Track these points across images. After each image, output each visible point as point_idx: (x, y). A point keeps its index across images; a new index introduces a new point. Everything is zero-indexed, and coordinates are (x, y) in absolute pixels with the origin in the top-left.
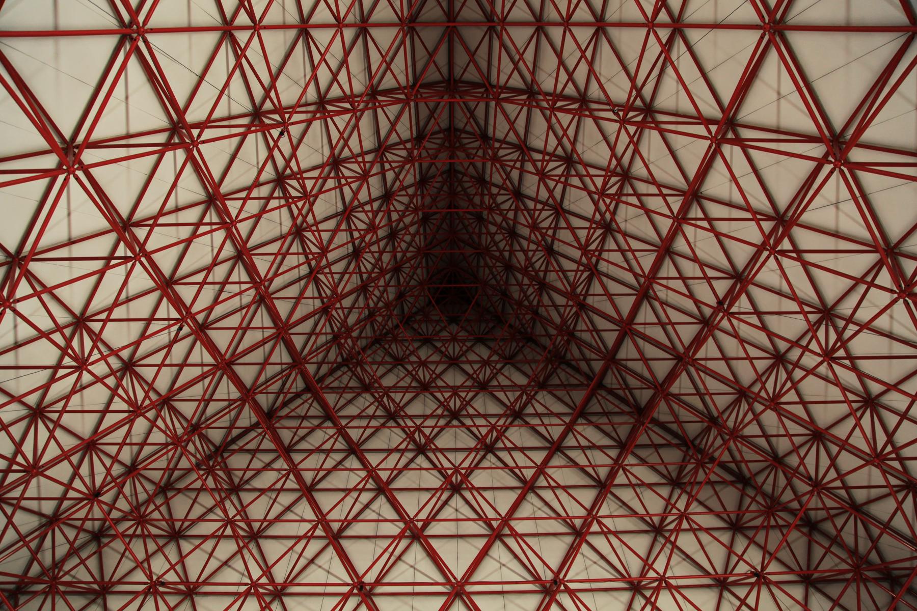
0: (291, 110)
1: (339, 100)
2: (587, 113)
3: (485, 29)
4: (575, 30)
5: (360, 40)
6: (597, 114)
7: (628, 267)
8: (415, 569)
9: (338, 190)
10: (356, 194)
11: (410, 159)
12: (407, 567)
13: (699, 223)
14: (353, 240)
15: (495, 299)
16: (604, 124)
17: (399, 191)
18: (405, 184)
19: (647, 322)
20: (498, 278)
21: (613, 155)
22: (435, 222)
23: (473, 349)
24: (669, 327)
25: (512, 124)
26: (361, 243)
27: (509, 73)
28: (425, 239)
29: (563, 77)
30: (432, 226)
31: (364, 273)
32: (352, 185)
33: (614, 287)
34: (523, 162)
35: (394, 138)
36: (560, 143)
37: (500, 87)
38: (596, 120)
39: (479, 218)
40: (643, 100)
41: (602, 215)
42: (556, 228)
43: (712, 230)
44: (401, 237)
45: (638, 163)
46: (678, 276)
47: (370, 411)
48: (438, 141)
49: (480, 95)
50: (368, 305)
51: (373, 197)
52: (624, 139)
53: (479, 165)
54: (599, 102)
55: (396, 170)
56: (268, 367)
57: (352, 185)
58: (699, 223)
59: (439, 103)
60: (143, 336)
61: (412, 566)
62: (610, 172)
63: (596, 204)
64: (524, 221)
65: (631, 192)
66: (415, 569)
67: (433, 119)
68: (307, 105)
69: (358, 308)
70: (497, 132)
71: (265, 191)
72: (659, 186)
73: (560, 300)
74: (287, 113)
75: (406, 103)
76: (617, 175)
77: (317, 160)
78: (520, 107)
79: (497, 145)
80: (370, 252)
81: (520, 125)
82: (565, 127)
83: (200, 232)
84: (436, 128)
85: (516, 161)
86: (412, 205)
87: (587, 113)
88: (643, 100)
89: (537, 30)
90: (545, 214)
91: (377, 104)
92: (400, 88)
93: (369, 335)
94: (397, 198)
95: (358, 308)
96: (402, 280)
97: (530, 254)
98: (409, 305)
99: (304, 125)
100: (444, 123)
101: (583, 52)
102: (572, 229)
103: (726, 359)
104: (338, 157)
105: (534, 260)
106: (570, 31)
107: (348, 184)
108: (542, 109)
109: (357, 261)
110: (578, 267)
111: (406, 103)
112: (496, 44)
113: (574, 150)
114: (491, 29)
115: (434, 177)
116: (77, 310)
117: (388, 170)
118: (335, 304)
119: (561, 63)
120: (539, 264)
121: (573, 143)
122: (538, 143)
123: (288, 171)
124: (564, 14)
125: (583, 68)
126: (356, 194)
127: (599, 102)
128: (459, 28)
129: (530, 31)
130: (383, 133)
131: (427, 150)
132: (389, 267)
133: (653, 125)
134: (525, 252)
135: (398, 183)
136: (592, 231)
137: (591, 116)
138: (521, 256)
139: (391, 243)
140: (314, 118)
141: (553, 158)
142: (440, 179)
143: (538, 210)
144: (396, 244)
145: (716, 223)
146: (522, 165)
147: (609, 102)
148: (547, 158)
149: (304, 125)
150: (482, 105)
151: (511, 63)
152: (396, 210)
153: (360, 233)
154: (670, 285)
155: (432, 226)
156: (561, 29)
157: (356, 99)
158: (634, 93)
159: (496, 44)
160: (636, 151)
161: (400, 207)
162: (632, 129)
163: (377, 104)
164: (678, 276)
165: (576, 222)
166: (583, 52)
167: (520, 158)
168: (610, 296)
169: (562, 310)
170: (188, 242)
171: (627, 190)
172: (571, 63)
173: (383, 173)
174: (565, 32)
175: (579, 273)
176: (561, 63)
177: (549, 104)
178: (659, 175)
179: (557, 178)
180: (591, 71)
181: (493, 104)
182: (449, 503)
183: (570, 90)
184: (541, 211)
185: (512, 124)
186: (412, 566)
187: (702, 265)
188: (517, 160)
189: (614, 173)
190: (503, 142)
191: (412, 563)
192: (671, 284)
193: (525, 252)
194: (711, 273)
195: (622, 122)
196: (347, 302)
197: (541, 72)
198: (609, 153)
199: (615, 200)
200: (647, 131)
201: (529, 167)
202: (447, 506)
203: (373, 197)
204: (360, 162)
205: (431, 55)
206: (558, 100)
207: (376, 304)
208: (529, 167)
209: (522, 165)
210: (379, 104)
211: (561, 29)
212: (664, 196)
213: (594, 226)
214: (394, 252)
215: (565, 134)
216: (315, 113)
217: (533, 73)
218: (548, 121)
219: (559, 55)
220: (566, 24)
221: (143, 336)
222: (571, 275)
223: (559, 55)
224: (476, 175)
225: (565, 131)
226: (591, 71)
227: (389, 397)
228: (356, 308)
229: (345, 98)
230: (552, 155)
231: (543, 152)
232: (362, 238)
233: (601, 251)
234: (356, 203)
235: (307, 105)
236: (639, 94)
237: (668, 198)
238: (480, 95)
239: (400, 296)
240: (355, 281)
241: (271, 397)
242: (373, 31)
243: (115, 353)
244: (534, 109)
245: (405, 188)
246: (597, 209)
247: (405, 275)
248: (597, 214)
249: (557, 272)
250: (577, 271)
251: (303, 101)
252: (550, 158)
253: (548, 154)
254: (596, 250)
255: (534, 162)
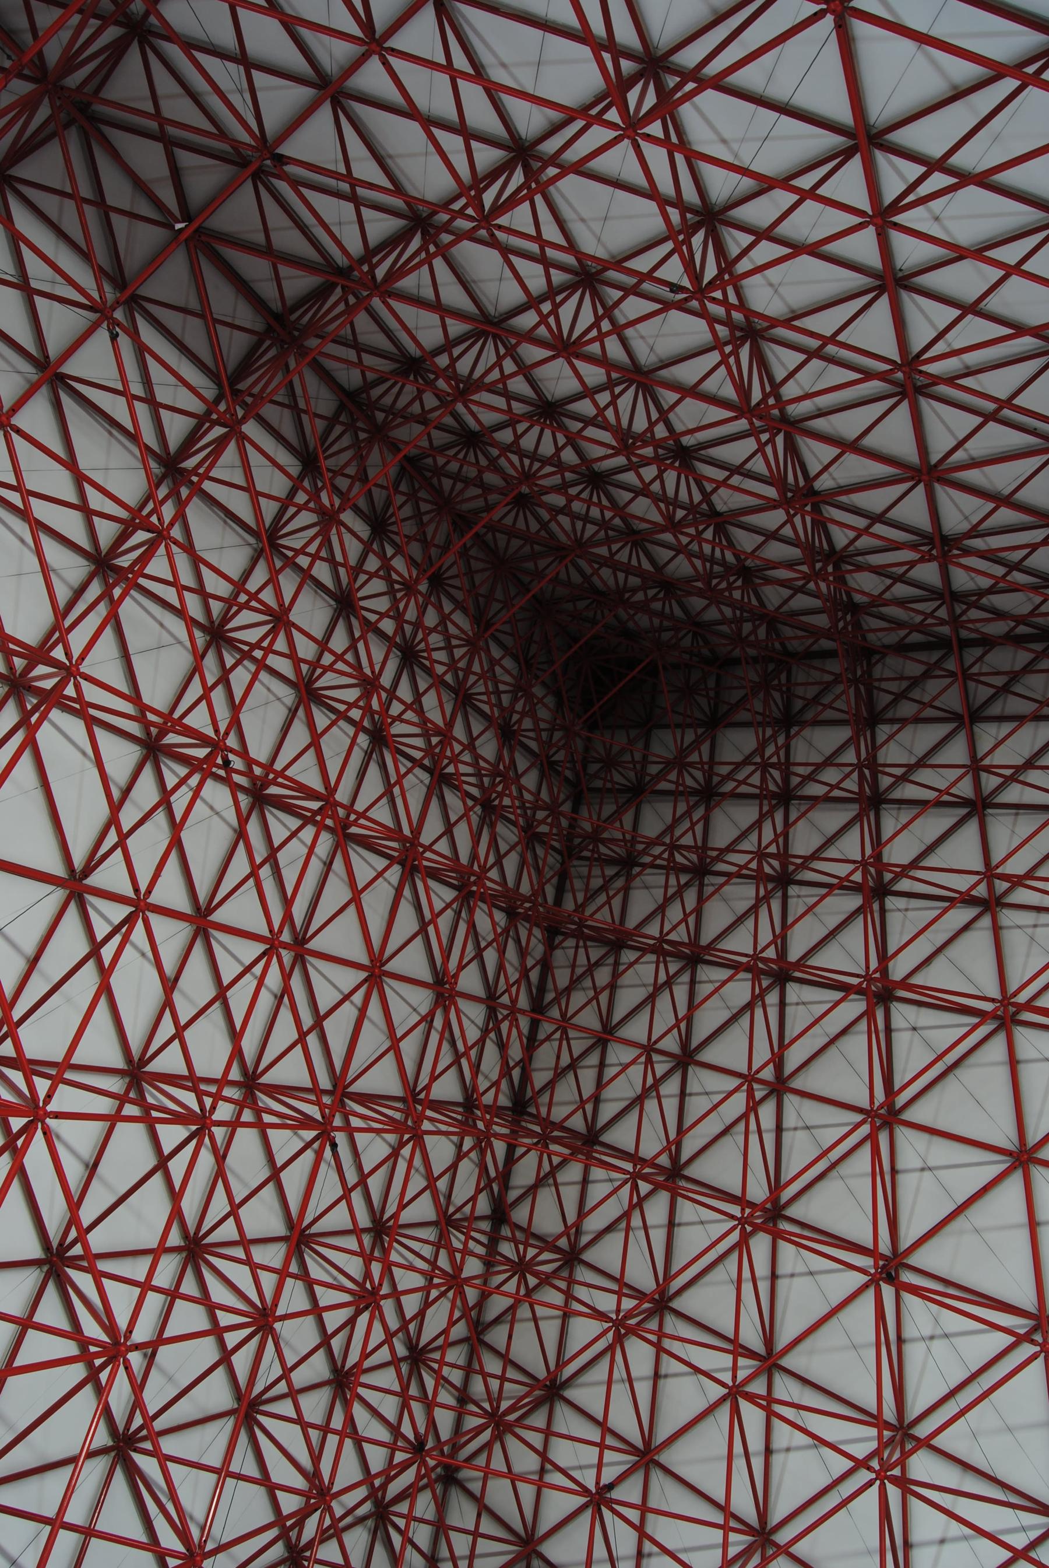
0: (57, 635)
1: (123, 537)
2: (552, 171)
3: (248, 186)
4: (397, 42)
5: (66, 400)
6: (572, 155)
7: (859, 376)
8: (930, 1169)
9: (263, 676)
10: (292, 655)
11: (328, 519)
12: (917, 1174)
13: (923, 190)
14: (357, 725)
15: (623, 556)
16: (602, 164)
17: (355, 580)
18: (353, 561)
19: (961, 437)
20: (595, 512)
21: (663, 202)
22: (454, 571)
23: (717, 759)
24: (1006, 412)
25: (437, 306)
26: (373, 719)
27: (729, 1121)
28: (465, 611)
29: (452, 143)
30: (456, 582)
31: (423, 758)
32: (276, 647)
33: (849, 424)
34: (512, 352)
35: (269, 509)
36: (547, 264)
37: (362, 261)
38: (579, 168)
39: (522, 502)
40: (630, 55)
41: (728, 322)
42: (664, 416)
43: (964, 179)
44: (422, 646)
45: (714, 176)
46: (958, 312)
47: (596, 883)
48: (346, 441)
49: (341, 307)
50: (468, 795)
51: (320, 638)
52: (657, 157)
53: (448, 420)
54: (555, 129)
55: (323, 554)
56: (423, 1183)
57: (276, 647)
58: (923, 190)
59: (291, 383)
60: (176, 1196)
61: (923, 1170)
62: (680, 232)
63: (703, 314)
64: (601, 451)
65: (746, 239)
66: (930, 1169)
67: (303, 416)
68: (79, 592)
69: (489, 944)
70: (421, 337)
71: (146, 792)
72: (785, 183)
73: (772, 519)
74: (35, 709)
75: (234, 432)
76: (694, 229)
77: (180, 660)
78: (426, 268)
79: (443, 361)
80: (395, 719)
81: (453, 295)
82: (533, 232)
83: (107, 959)
84: (320, 424)
85: (499, 364)
86: (397, 586)
87: (552, 171)
88: (630, 55)
89: (336, 105)
90: (625, 402)
91: (195, 479)
92: (202, 421)
93: (514, 839)
94: (360, 594)
95: (489, 944)
96: (486, 708)
97: (656, 487)
98: (532, 734)
99: (109, 632)
100: (324, 402)
101: (448, 68)
102: (693, 392)
103: (972, 309)
104: (212, 622)
105: (670, 491)
106: (393, 51)
107: (269, 650)
108: (470, 236)
109: (387, 747)
110: (758, 441)
111: (234, 432)
112: (299, 911)
113: (580, 256)
114: (259, 177)
115: (388, 503)
116: (33, 1250)
117: (311, 565)
118: (418, 852)
119: (428, 123)
120: (687, 493)
121: (571, 247)
122: (510, 295)
123: (154, 731)
124: (356, 31)
125: (473, 94)
126: (292, 655)
127: (555, 129)
128: (206, 224)
129: (325, 115)
130: (248, 517)
131: (340, 472)
132: (448, 709)
133: (690, 86)
134: (644, 491)
135: (342, 571)
136: (732, 360)
137: (566, 170)
138: (642, 507)
139: (416, 669)
140: (115, 605)
141: (559, 299)
142: (399, 499)
143: (607, 407)
144: (427, 663)
145: (958, 160)
146: (517, 360)
147: (570, 114)
148: (546, 307)
149: (109, 632)
150: (362, 320)
151: (343, 202)
152: (382, 616)
153: (359, 707)
154: (957, 345)
155: (456, 582)
156: (374, 63)
157: (145, 513)
158: (607, 56)
159: (299, 911)
160: (693, 157)
161: (382, 604)
162: (655, 129)
163: (195, 479)
164: (957, 313)
165: (688, 373)
166: (448, 68)
167: (502, 351)
168: (853, 447)
169: (787, 531)
170: (105, 989)
171: (738, 244)
172: (443, 106)
173: (306, 576)
174: (386, 64)
175: (769, 449)
176: (428, 123)
177: (470, 218)
178: (769, 164)
179: (594, 333)
180: (493, 91)
181: (376, 302)
182: (893, 1026)
183: (486, 156)
184: (613, 402)
185: (437, 306)
186: (923, 1170)
187: (979, 253)
188: (500, 359)
189: (690, 230)
190: (448, 345)
191: (919, 1164)
192: (957, 339)
193: (644, 491)
194: (1010, 254)
195: (630, 133)
196: (433, 827)
197: (400, 162)
198: (652, 206)
199: (728, 283)
200: (686, 111)
201: (532, 353)
202: (894, 1035)
203: (320, 638)
204: (248, 602)
205: (205, 314)
206: (481, 192)
207: (480, 786)
208: (532, 353)
209: (517, 360)
210: (197, 475)
211: (374, 64)
212: (811, 194)
213: (728, 349)
214: (438, 682)
215: (543, 244)
216: (107, 594)
217: (398, 190)
218: (493, 243)
219: (411, 112)
220: (374, 47)
221: (176, 1196)
222: (758, 465)
223: (411, 112)
224: (452, 438)
225: (538, 238)
226: (493, 91)
227: (604, 842)
228: (486, 947)
229: (128, 528)
230: (552, 292)
231: (532, 302)
232: (367, 710)
233: (776, 387)
234: (304, 668)
235: (79, 592)
236: (619, 52)
237: (822, 191)
238: (341, 307)
239: (507, 735)
240: (416, 784)
241: (452, 1074)
242: (69, 368)
243: (223, 1082)
244: (454, 250)
245: (357, 570)
246: (712, 321)
247: (484, 698)
248: (718, 327)
249: (724, 483)
250: (761, 449)
251: (63, 595)
252: (554, 303)
253: (542, 298)
254: (765, 396)
255: (529, 337)
